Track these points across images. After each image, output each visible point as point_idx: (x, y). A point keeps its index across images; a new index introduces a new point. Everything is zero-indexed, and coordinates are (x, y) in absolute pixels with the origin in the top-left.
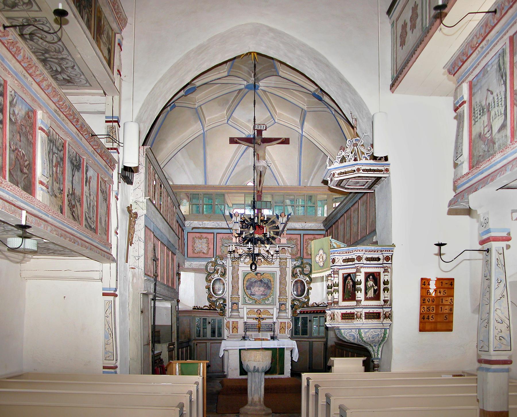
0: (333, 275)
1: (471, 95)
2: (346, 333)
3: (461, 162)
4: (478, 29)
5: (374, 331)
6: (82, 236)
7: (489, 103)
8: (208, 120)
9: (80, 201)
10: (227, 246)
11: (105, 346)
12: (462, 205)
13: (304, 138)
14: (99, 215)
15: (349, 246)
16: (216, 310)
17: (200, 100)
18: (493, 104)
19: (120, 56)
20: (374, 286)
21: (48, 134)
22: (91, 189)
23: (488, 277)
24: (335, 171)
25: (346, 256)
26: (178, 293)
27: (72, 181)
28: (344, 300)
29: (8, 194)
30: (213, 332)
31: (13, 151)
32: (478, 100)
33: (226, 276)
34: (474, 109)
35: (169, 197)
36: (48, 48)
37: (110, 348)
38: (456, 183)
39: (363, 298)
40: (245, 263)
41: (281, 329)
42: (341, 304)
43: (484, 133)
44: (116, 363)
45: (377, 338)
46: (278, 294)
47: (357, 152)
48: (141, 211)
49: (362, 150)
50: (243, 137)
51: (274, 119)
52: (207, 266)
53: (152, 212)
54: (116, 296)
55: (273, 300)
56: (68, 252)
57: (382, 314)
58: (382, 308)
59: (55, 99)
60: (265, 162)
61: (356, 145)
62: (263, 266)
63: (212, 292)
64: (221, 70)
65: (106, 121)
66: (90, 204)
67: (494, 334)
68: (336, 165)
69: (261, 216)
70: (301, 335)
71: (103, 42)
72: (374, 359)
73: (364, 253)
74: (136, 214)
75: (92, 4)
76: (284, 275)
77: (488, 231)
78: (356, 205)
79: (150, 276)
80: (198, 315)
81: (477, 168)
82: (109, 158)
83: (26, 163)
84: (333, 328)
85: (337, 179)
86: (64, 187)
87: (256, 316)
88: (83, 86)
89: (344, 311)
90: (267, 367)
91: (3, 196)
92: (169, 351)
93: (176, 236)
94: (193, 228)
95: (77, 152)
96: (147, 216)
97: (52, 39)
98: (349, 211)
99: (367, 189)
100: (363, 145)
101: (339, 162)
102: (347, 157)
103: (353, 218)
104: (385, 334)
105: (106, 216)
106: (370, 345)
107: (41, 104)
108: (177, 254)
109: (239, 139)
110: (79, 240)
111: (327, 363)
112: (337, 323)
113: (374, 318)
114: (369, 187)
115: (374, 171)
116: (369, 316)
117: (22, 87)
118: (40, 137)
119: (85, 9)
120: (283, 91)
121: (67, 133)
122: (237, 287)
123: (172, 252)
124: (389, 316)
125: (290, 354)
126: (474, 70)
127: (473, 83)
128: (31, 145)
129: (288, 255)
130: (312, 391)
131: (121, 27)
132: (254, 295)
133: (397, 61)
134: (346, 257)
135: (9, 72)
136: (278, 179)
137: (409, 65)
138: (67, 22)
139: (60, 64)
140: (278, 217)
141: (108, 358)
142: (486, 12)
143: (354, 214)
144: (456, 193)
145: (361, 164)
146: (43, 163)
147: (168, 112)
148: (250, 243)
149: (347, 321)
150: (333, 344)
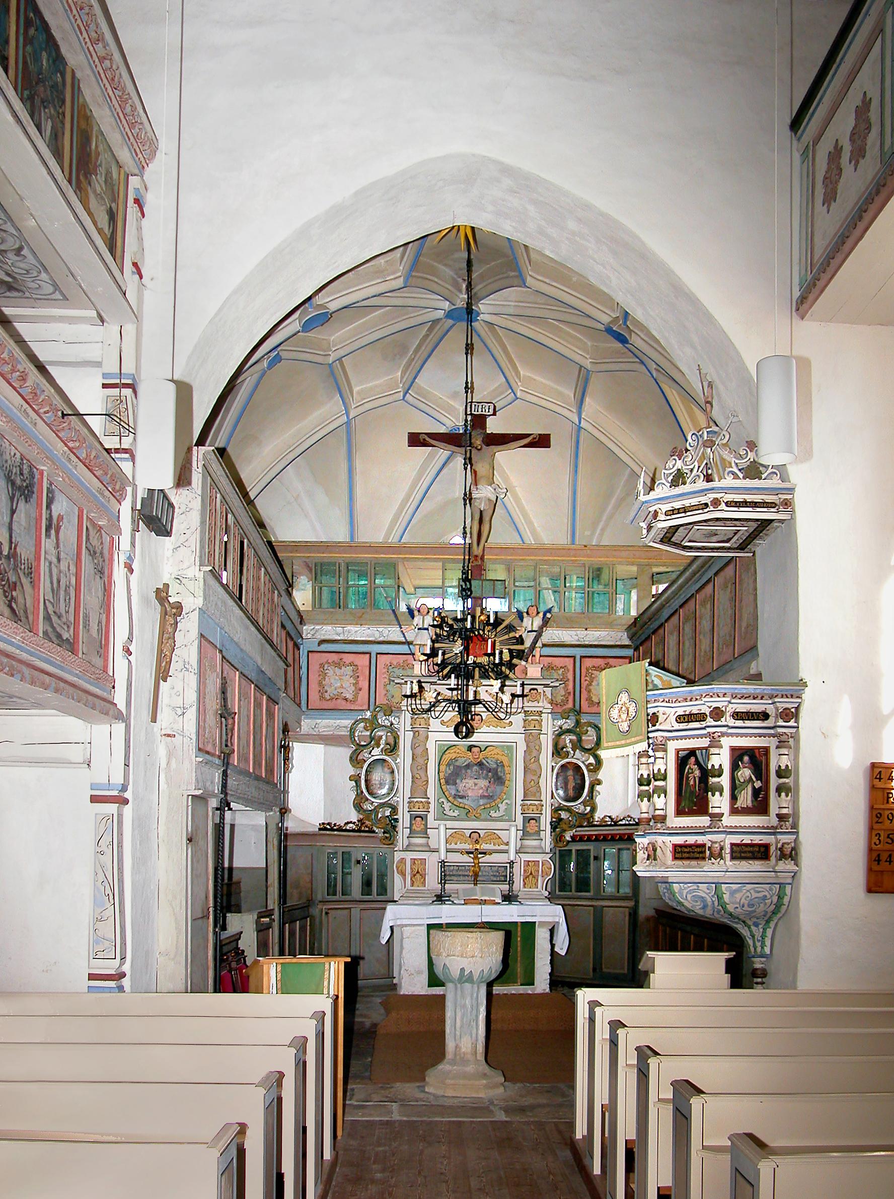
0: (651, 753)
2: (685, 892)
6: (34, 659)
8: (358, 393)
9: (32, 573)
15: (691, 682)
16: (374, 832)
19: (139, 229)
20: (754, 779)
22: (61, 545)
26: (285, 792)
28: (679, 812)
30: (367, 884)
35: (263, 569)
40: (443, 723)
41: (528, 876)
44: (121, 965)
45: (762, 905)
47: (711, 460)
52: (352, 730)
53: (219, 603)
54: (126, 802)
57: (772, 849)
58: (774, 834)
60: (493, 491)
63: (365, 791)
64: (389, 275)
66: (59, 582)
68: (662, 490)
69: (482, 613)
70: (574, 893)
71: (95, 191)
72: (753, 957)
73: (730, 702)
74: (179, 607)
75: (65, 97)
76: (534, 751)
79: (213, 755)
80: (331, 844)
82: (110, 473)
85: (663, 524)
87: (468, 847)
89: (679, 840)
90: (493, 972)
92: (259, 931)
93: (278, 659)
95: (24, 454)
98: (692, 602)
99: (737, 548)
100: (725, 445)
101: (668, 485)
103: (701, 618)
104: (780, 898)
105: (102, 611)
106: (744, 922)
108: (281, 701)
111: (638, 964)
113: (754, 858)
114: (740, 544)
115: (755, 505)
116: (741, 852)
119: (45, 107)
122: (424, 779)
123: (269, 697)
125: (549, 938)
129: (544, 705)
130: (602, 1033)
131: (142, 159)
132: (462, 797)
134: (685, 711)
136: (523, 529)
140: (520, 615)
141: (100, 955)
143: (703, 610)
145: (722, 488)
147: (264, 373)
148: (453, 676)
149: (686, 862)
150: (652, 913)
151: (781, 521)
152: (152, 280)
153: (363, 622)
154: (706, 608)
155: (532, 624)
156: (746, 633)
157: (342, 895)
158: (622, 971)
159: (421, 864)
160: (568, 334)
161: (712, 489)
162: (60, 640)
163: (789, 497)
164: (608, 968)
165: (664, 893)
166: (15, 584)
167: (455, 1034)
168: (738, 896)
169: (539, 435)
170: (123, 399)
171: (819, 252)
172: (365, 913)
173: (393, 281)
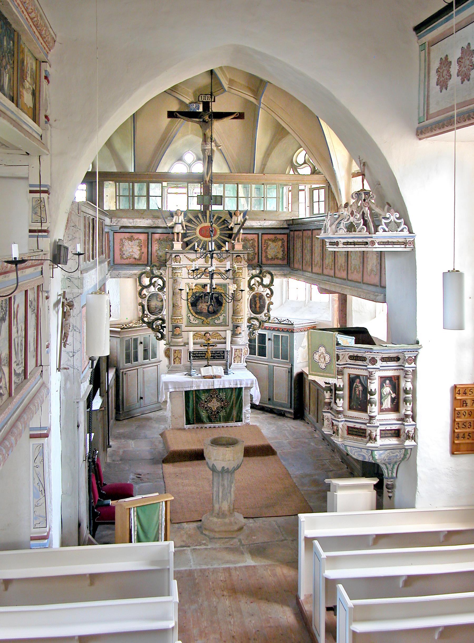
2: (353, 451)
5: (391, 452)
11: (34, 509)
20: (392, 393)
25: (354, 353)
33: (165, 290)
55: (224, 320)
94: (122, 227)
149: (355, 437)
152: (55, 121)
153: (144, 217)
155: (237, 220)
158: (285, 402)
164: (277, 399)
167: (219, 501)
168: (383, 456)
170: (42, 199)
172: (144, 369)
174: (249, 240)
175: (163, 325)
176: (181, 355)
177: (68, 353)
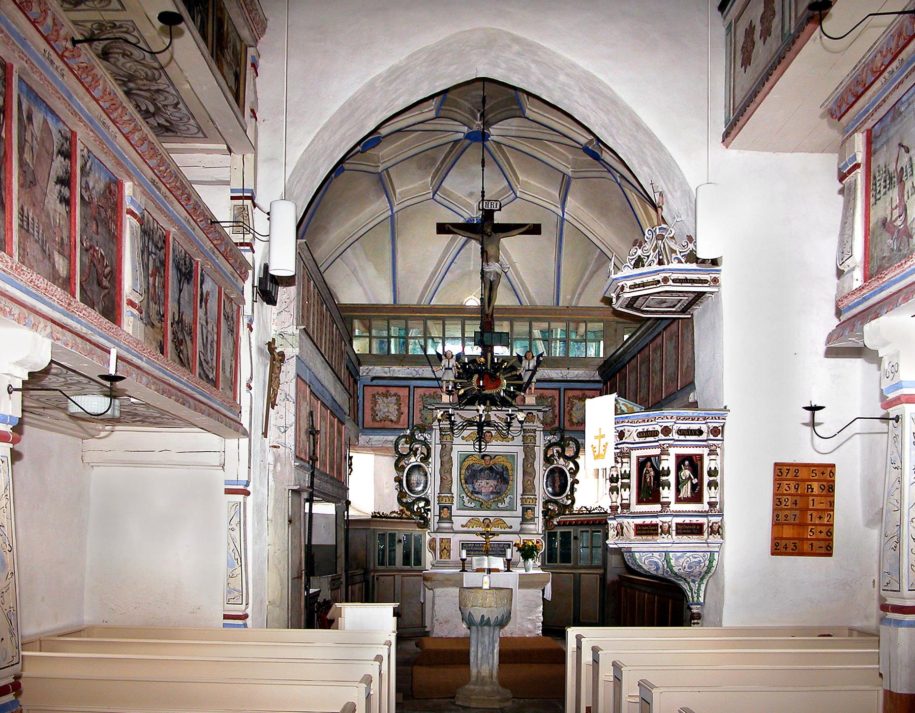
1: (869, 154)
2: (643, 558)
3: (849, 269)
4: (884, 41)
5: (692, 555)
6: (194, 393)
7: (902, 168)
9: (192, 333)
10: (432, 409)
12: (850, 341)
13: (566, 224)
14: (221, 357)
15: (648, 409)
17: (386, 160)
18: (909, 170)
19: (255, 85)
20: (693, 477)
21: (141, 221)
23: (898, 464)
24: (626, 282)
27: (179, 299)
28: (640, 501)
29: (79, 322)
30: (406, 559)
31: (87, 250)
32: (881, 162)
33: (430, 460)
34: (875, 178)
36: (134, 72)
37: (236, 583)
38: (840, 303)
39: (672, 498)
40: (463, 438)
42: (634, 508)
43: (891, 219)
46: (520, 491)
47: (662, 249)
48: (291, 352)
49: (671, 246)
50: (460, 222)
51: (514, 192)
54: (248, 494)
56: (168, 419)
57: (705, 527)
58: (706, 516)
59: (153, 163)
61: (661, 237)
62: (494, 442)
63: (406, 488)
64: (425, 109)
65: (231, 197)
66: (207, 338)
67: (908, 561)
68: (627, 272)
73: (675, 423)
74: (282, 354)
76: (530, 458)
77: (898, 386)
78: (659, 340)
81: (878, 278)
82: (239, 261)
83: (107, 270)
84: (619, 551)
85: (628, 295)
86: (166, 310)
87: (481, 529)
88: (193, 137)
89: (639, 521)
91: (72, 327)
94: (374, 378)
96: (299, 359)
97: (142, 57)
98: (646, 350)
100: (673, 238)
101: (632, 267)
102: (646, 258)
104: (711, 562)
106: (685, 579)
107: (131, 171)
109: (453, 225)
110: (190, 400)
112: (628, 542)
113: (692, 533)
114: (683, 309)
115: (693, 281)
117: (100, 142)
118: (129, 225)
120: (531, 144)
121: (173, 220)
123: (339, 420)
124: (718, 529)
126: (876, 111)
127: (873, 133)
128: (115, 240)
129: (538, 425)
130: (587, 657)
132: (477, 493)
133: (736, 92)
134: (643, 429)
135: (80, 118)
137: (758, 99)
138: (181, 33)
139: (154, 100)
140: (519, 358)
142: (899, 13)
144: (840, 321)
145: (670, 270)
146: (134, 270)
149: (644, 537)
150: (616, 578)
151: (712, 293)
154: (656, 354)
156: (686, 372)
157: (389, 565)
159: (447, 542)
160: (558, 152)
161: (663, 270)
162: (209, 380)
163: (716, 276)
165: (628, 559)
166: (182, 340)
169: (534, 224)
170: (246, 207)
171: (738, 100)
173: (428, 113)
174: (547, 398)
175: (426, 508)
176: (450, 546)
177: (279, 428)
